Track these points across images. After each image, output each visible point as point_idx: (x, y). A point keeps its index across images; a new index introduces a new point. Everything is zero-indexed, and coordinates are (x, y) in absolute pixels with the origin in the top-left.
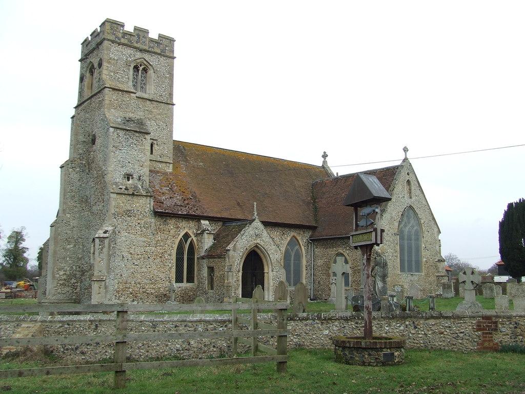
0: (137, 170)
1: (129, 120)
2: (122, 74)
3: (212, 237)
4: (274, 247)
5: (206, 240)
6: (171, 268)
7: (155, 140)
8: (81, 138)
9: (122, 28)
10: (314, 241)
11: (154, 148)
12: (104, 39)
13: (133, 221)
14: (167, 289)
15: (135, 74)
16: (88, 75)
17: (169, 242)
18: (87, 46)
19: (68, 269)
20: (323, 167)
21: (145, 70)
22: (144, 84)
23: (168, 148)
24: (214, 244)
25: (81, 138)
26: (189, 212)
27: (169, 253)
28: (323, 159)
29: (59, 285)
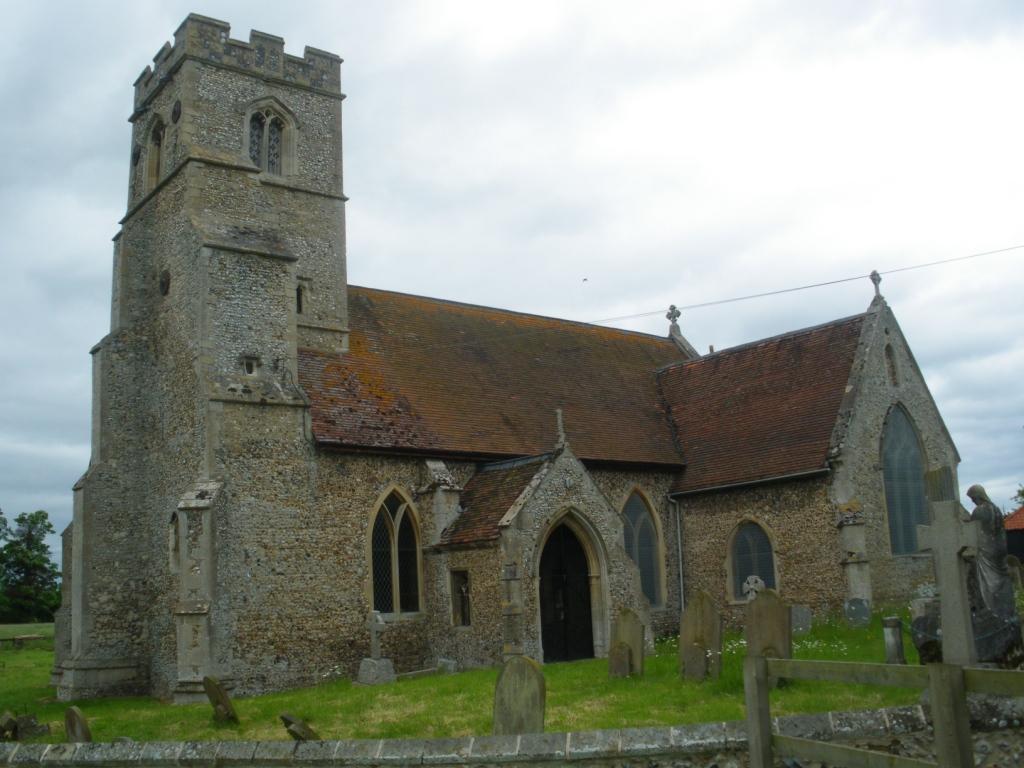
1: (247, 232)
2: (226, 132)
3: (455, 499)
4: (603, 513)
5: (444, 507)
6: (361, 578)
7: (306, 279)
8: (136, 283)
9: (223, 34)
11: (303, 299)
14: (356, 628)
15: (256, 133)
16: (150, 145)
17: (353, 515)
19: (119, 588)
20: (671, 338)
21: (278, 125)
22: (277, 155)
23: (335, 297)
24: (462, 516)
25: (136, 283)
26: (397, 442)
27: (355, 541)
28: (669, 323)
29: (99, 625)
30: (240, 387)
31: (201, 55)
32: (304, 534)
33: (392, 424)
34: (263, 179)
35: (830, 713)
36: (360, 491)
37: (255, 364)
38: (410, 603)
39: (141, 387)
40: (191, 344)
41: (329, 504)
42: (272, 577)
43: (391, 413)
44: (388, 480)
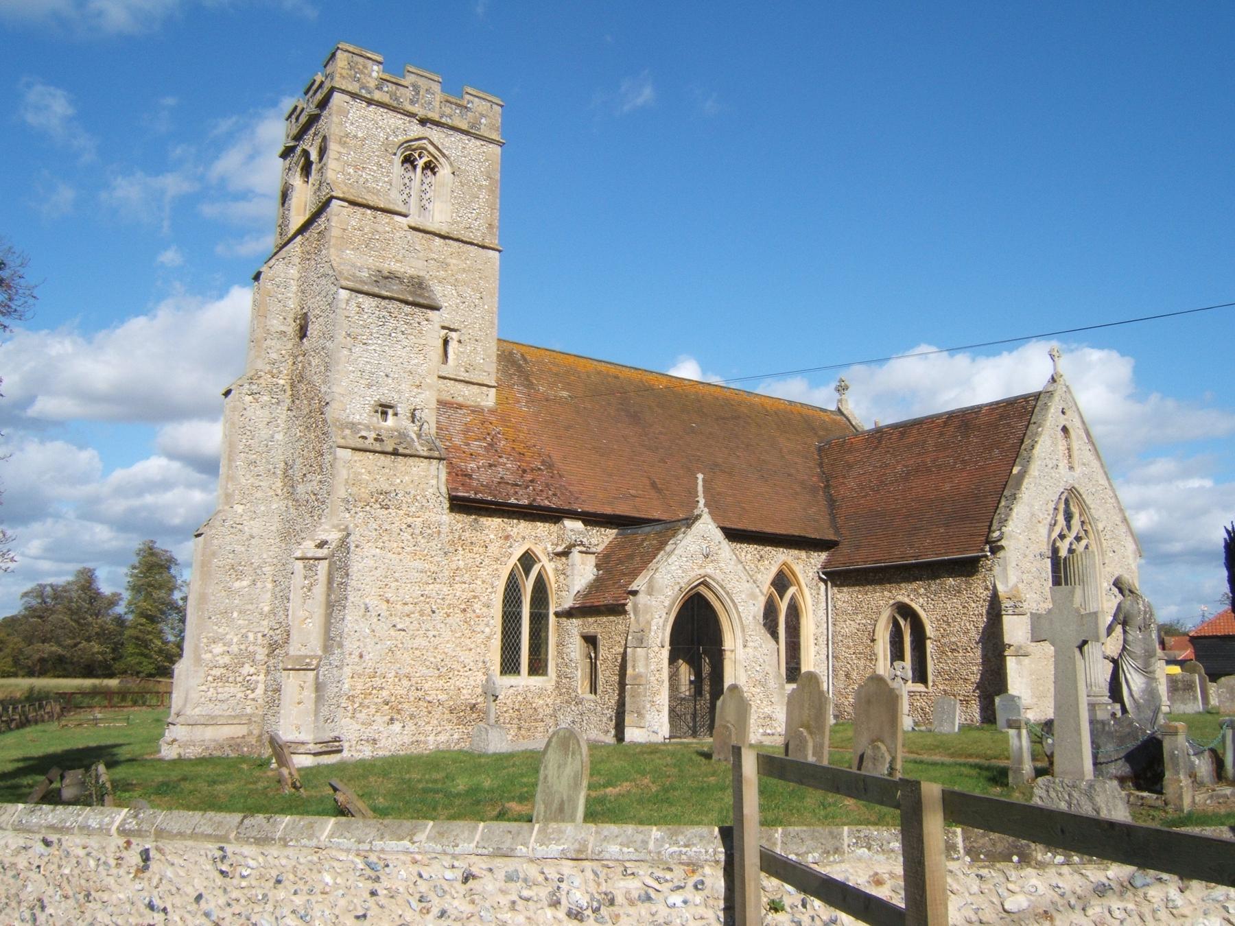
0: (405, 397)
1: (391, 277)
3: (591, 560)
10: (835, 577)
12: (332, 90)
13: (396, 519)
17: (483, 573)
18: (297, 119)
21: (430, 167)
29: (210, 678)
30: (373, 435)
31: (350, 89)
32: (431, 589)
33: (532, 481)
34: (413, 225)
35: (780, 830)
36: (494, 549)
37: (390, 412)
38: (537, 667)
39: (275, 432)
40: (323, 389)
41: (460, 559)
42: (392, 633)
43: (532, 470)
44: (524, 538)
